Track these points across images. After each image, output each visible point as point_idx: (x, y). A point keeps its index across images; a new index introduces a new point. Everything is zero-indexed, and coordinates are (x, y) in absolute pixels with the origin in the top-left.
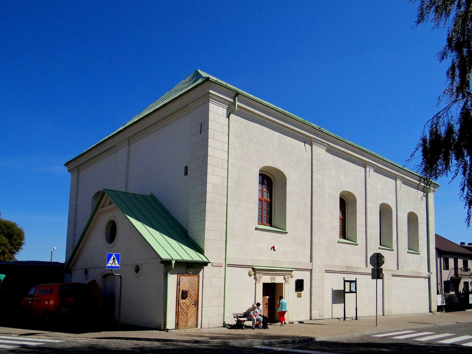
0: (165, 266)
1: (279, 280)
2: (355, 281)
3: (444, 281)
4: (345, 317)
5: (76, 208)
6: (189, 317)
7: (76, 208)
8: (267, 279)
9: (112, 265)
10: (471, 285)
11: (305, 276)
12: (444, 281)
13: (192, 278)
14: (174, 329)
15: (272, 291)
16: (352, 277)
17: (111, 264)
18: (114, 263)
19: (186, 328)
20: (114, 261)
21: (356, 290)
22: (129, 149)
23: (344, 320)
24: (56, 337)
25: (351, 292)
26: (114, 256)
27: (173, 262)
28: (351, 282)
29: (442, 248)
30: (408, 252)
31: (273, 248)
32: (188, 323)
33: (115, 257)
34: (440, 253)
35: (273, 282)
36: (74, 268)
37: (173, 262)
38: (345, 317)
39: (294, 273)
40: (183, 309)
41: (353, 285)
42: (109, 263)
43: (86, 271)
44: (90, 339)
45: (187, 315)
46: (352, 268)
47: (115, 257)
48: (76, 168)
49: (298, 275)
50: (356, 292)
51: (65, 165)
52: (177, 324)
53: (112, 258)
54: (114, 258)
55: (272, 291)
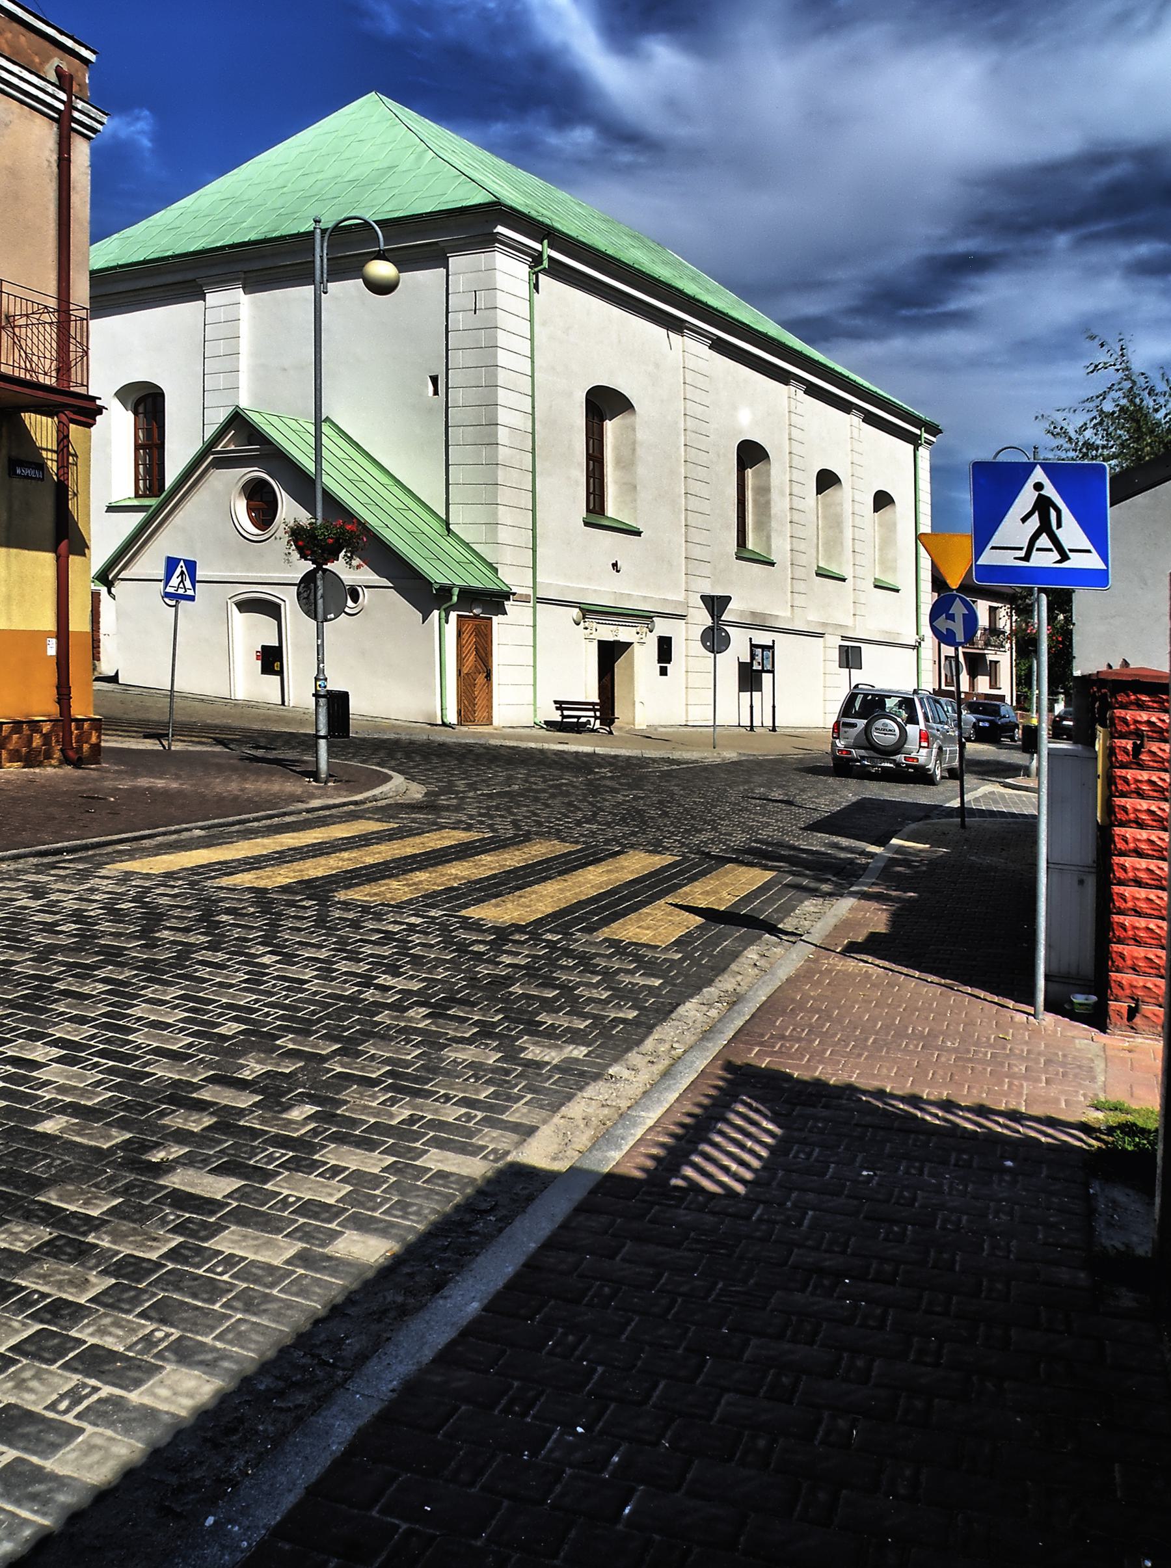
1: (624, 634)
4: (774, 726)
8: (608, 632)
9: (1027, 558)
10: (332, 616)
16: (763, 638)
17: (1022, 554)
18: (1044, 541)
26: (1038, 486)
27: (456, 591)
31: (615, 565)
33: (1050, 491)
35: (616, 638)
37: (456, 591)
38: (774, 726)
41: (768, 653)
42: (992, 543)
46: (764, 616)
47: (1050, 491)
49: (662, 627)
50: (772, 672)
53: (1026, 498)
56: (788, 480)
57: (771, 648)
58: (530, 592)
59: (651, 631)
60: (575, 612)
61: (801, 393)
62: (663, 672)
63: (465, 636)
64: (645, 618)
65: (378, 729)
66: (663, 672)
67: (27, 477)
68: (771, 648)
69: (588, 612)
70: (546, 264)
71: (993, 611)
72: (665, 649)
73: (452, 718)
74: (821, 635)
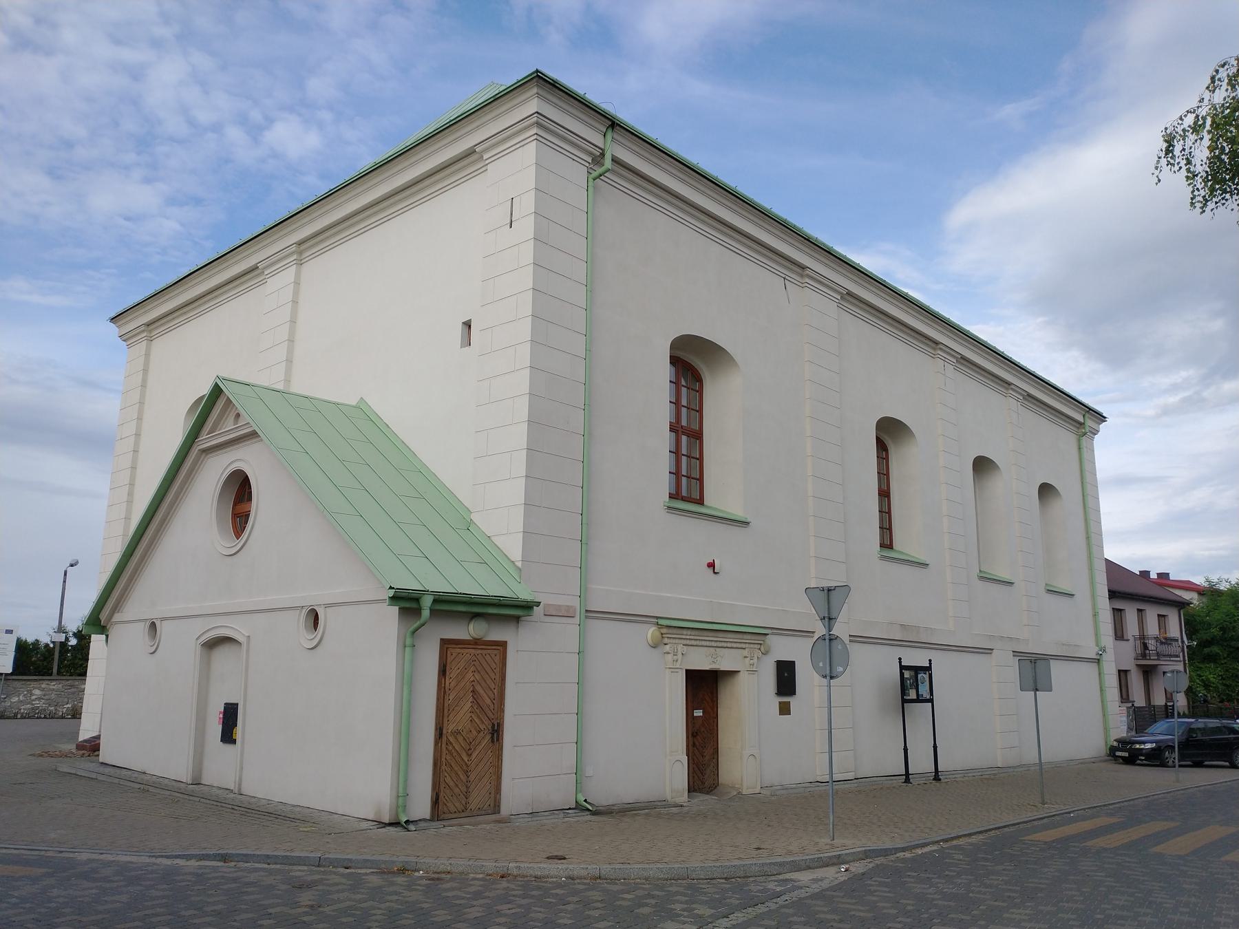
0: (404, 612)
2: (929, 669)
3: (504, 645)
4: (907, 774)
5: (137, 443)
6: (472, 777)
7: (137, 443)
8: (702, 661)
11: (798, 651)
12: (504, 645)
13: (484, 652)
14: (424, 820)
16: (916, 658)
19: (463, 814)
21: (932, 694)
22: (298, 275)
23: (907, 780)
25: (919, 700)
27: (427, 602)
28: (917, 670)
29: (1116, 588)
31: (711, 565)
32: (471, 799)
34: (1113, 595)
36: (117, 617)
37: (427, 602)
38: (907, 774)
39: (773, 640)
43: (913, 686)
45: (466, 772)
48: (143, 328)
49: (784, 649)
50: (931, 701)
51: (113, 319)
52: (436, 802)
56: (930, 472)
57: (928, 669)
58: (575, 603)
60: (651, 631)
61: (950, 368)
62: (785, 709)
63: (452, 674)
64: (757, 636)
65: (443, 190)
66: (785, 709)
67: (188, 857)
68: (928, 669)
69: (672, 630)
70: (608, 163)
71: (1161, 617)
73: (421, 806)
74: (988, 651)
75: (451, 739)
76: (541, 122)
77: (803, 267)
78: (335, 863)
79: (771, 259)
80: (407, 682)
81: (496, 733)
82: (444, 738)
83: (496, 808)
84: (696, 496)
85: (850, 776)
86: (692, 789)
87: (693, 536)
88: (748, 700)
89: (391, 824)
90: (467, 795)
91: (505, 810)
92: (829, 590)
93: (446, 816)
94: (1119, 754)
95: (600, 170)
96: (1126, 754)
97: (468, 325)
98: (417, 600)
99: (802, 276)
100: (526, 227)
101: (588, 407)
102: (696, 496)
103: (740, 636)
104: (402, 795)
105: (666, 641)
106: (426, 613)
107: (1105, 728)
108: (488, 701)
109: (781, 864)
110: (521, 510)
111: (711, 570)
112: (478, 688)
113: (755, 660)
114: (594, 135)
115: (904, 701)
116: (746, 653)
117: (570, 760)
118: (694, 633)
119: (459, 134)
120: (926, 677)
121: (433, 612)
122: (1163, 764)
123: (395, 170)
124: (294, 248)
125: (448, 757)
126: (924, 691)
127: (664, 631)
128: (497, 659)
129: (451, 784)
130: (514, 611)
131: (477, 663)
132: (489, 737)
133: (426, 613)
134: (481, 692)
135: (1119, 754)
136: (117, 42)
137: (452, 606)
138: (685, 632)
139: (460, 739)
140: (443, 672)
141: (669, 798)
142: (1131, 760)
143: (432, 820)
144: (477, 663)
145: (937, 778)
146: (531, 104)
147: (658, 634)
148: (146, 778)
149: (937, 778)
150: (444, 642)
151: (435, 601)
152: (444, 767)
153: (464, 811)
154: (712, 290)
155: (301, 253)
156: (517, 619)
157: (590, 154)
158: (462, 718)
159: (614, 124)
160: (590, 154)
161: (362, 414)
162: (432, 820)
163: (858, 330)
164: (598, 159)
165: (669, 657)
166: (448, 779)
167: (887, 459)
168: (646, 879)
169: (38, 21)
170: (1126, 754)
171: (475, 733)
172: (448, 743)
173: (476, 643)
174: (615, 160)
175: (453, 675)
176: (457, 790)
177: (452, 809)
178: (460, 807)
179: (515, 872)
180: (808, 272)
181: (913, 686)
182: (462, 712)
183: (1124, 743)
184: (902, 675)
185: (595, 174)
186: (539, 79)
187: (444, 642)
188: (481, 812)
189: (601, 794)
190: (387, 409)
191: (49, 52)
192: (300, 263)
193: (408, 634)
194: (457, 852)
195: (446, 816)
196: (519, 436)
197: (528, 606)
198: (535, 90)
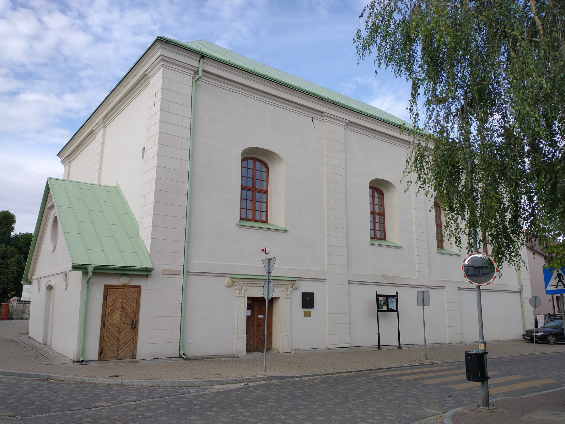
2: (396, 296)
3: (140, 287)
4: (379, 345)
6: (121, 343)
8: (257, 292)
9: (557, 288)
12: (140, 287)
15: (260, 309)
18: (560, 283)
20: (560, 280)
24: (343, 374)
25: (389, 310)
27: (90, 269)
28: (388, 297)
30: (372, 244)
32: (120, 353)
33: (560, 272)
37: (90, 269)
38: (379, 345)
39: (298, 283)
40: (111, 333)
44: (345, 374)
47: (560, 272)
49: (307, 288)
50: (397, 311)
52: (101, 353)
53: (555, 274)
54: (559, 275)
55: (260, 309)
57: (395, 296)
59: (296, 289)
64: (291, 282)
65: (140, 92)
68: (395, 296)
69: (237, 280)
72: (308, 301)
73: (93, 353)
75: (109, 327)
76: (163, 59)
77: (322, 112)
78: (25, 376)
79: (301, 109)
80: (86, 303)
81: (134, 325)
82: (106, 327)
83: (134, 356)
84: (264, 219)
85: (348, 345)
86: (249, 350)
87: (254, 238)
88: (287, 312)
89: (77, 362)
90: (118, 351)
91: (138, 357)
92: (269, 260)
93: (106, 359)
94: (526, 337)
95: (198, 77)
96: (529, 338)
97: (144, 149)
98: (86, 268)
99: (322, 116)
100: (158, 104)
101: (191, 182)
102: (264, 219)
103: (279, 281)
104: (83, 350)
105: (235, 284)
106: (90, 274)
107: (524, 326)
108: (130, 311)
109: (212, 382)
110: (150, 229)
111: (264, 252)
112: (125, 305)
113: (289, 292)
114: (194, 62)
115: (378, 311)
116: (283, 289)
117: (176, 335)
118: (251, 280)
119: (140, 67)
120: (394, 300)
121: (94, 273)
122: (548, 343)
123: (125, 84)
124: (101, 121)
125: (108, 334)
126: (392, 306)
127: (234, 280)
128: (135, 293)
129: (109, 346)
130: (145, 273)
131: (124, 295)
132: (130, 326)
133: (90, 274)
134: (127, 307)
135: (526, 337)
136: (135, 34)
137: (101, 271)
138: (246, 280)
139: (115, 327)
140: (105, 298)
141: (235, 354)
142: (531, 340)
143: (99, 360)
144: (124, 295)
145: (400, 347)
146: (159, 51)
147: (231, 281)
148: (33, 342)
149: (400, 347)
150: (106, 286)
151: (95, 269)
152: (105, 338)
153: (117, 357)
154: (265, 126)
155: (105, 123)
156: (147, 276)
157: (193, 70)
158: (116, 317)
159: (203, 56)
160: (193, 70)
161: (116, 190)
162: (99, 360)
163: (358, 139)
164: (196, 72)
165: (237, 292)
166: (108, 344)
167: (383, 198)
168: (141, 386)
169: (105, 29)
170: (529, 337)
171: (122, 324)
172: (108, 328)
173: (124, 286)
174: (204, 71)
175: (111, 299)
176: (112, 348)
177: (109, 356)
178: (114, 356)
179: (87, 381)
180: (324, 114)
181: (385, 304)
182: (115, 316)
183: (529, 332)
184: (378, 299)
185: (196, 79)
186: (160, 40)
187: (106, 286)
188: (125, 357)
189: (191, 352)
190: (124, 189)
191: (109, 42)
192: (105, 127)
193: (85, 283)
194: (127, 375)
195: (106, 359)
196: (151, 197)
197: (149, 271)
198: (159, 45)
